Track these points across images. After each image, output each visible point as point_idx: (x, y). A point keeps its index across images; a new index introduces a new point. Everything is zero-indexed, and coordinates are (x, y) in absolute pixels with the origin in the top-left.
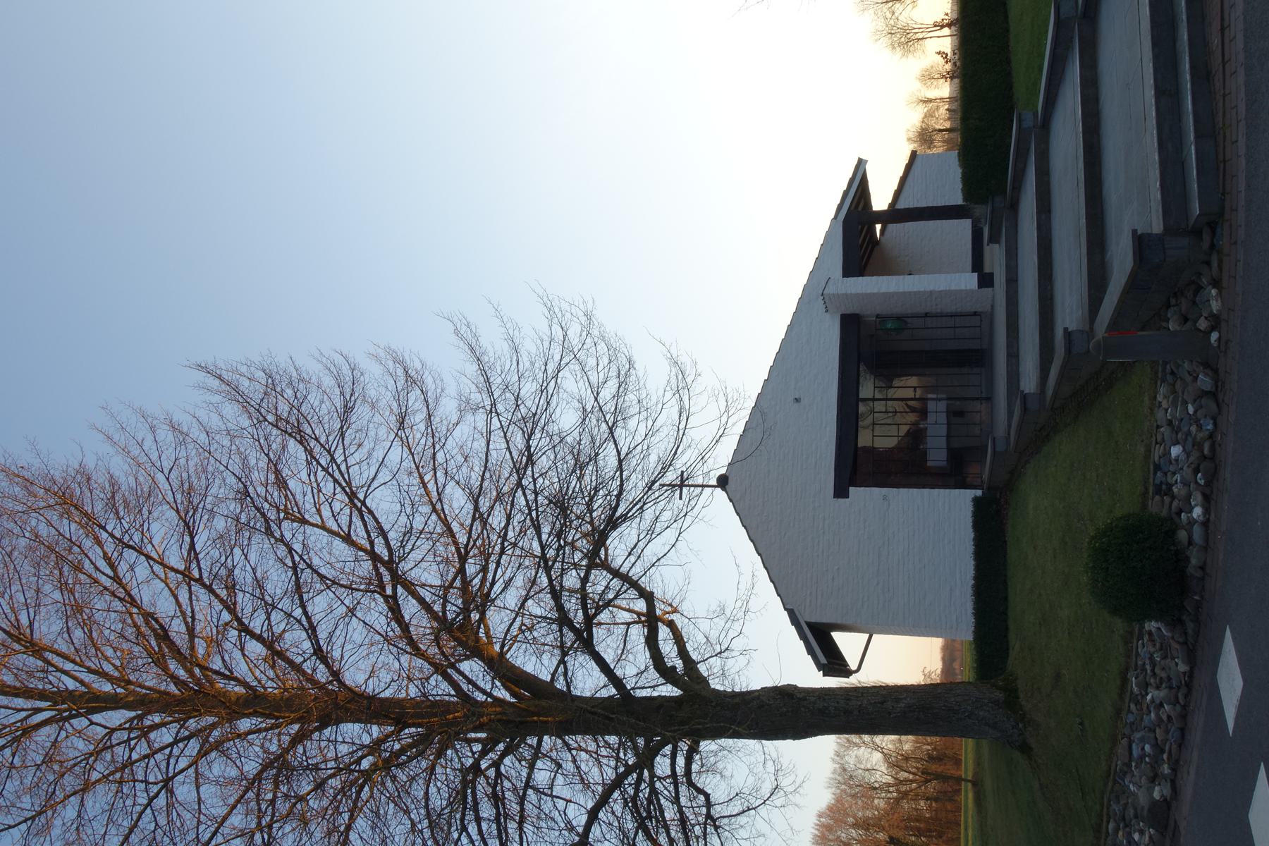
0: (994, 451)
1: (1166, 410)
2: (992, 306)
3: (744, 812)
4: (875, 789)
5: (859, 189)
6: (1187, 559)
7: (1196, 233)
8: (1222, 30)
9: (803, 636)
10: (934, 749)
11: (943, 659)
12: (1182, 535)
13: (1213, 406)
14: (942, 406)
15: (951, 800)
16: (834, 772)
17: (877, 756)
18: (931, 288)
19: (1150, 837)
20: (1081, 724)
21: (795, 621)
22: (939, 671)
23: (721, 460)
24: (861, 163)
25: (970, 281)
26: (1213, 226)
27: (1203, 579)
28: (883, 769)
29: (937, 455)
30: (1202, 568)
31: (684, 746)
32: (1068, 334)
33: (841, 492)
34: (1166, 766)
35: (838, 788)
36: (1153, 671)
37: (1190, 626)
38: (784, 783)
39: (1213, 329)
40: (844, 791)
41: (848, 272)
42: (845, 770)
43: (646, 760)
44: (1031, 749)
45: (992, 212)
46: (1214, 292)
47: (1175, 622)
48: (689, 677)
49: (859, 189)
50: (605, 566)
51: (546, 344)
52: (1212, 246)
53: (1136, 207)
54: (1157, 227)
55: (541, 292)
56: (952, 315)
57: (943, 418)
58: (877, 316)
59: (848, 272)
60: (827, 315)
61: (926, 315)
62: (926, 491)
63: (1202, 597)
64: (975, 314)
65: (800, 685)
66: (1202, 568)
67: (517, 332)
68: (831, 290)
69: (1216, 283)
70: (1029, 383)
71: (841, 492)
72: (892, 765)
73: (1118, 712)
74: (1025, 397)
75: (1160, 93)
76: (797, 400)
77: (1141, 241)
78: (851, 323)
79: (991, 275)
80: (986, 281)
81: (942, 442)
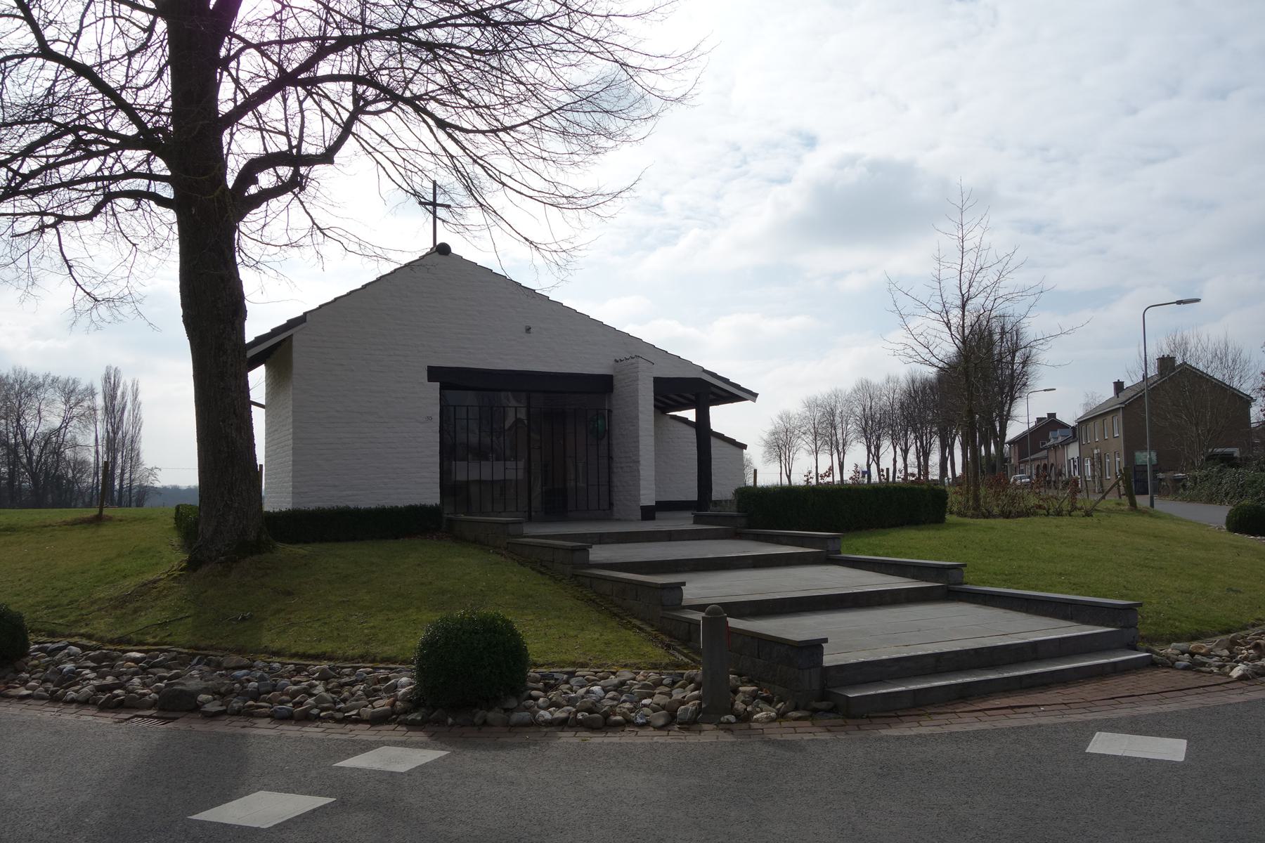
0: (507, 523)
1: (634, 679)
2: (619, 520)
3: (66, 261)
4: (18, 421)
5: (730, 393)
6: (490, 709)
7: (824, 695)
8: (1012, 708)
9: (276, 332)
10: (68, 480)
11: (165, 488)
12: (513, 703)
13: (661, 722)
14: (511, 475)
15: (922, 423)
16: (33, 377)
17: (57, 422)
18: (642, 462)
19: (145, 695)
20: (244, 619)
21: (292, 324)
22: (157, 485)
23: (459, 247)
24: (754, 396)
25: (648, 497)
26: (834, 710)
27: (474, 725)
28: (42, 429)
29: (464, 471)
30: (485, 723)
31: (167, 191)
32: (678, 587)
33: (434, 373)
34: (241, 704)
35: (16, 380)
36: (346, 684)
37: (416, 716)
38: (102, 309)
39: (737, 716)
40: (12, 387)
41: (658, 382)
42: (37, 388)
43: (146, 140)
44: (195, 570)
45: (732, 517)
46: (773, 714)
47: (414, 702)
48: (243, 202)
49: (730, 393)
50: (360, 107)
51: (620, 54)
52: (815, 711)
53: (851, 639)
54: (829, 660)
55: (703, 48)
56: (610, 482)
57: (498, 476)
58: (610, 411)
59: (658, 382)
60: (612, 362)
61: (610, 458)
62: (437, 459)
63: (452, 725)
64: (611, 504)
65: (246, 323)
66: (485, 723)
67: (659, 17)
68: (642, 365)
69: (781, 716)
70: (599, 554)
71: (434, 373)
72: (47, 439)
73: (277, 653)
74: (585, 550)
75: (938, 657)
76: (528, 330)
77: (815, 647)
78: (602, 385)
79: (653, 518)
80: (647, 514)
81: (474, 476)
